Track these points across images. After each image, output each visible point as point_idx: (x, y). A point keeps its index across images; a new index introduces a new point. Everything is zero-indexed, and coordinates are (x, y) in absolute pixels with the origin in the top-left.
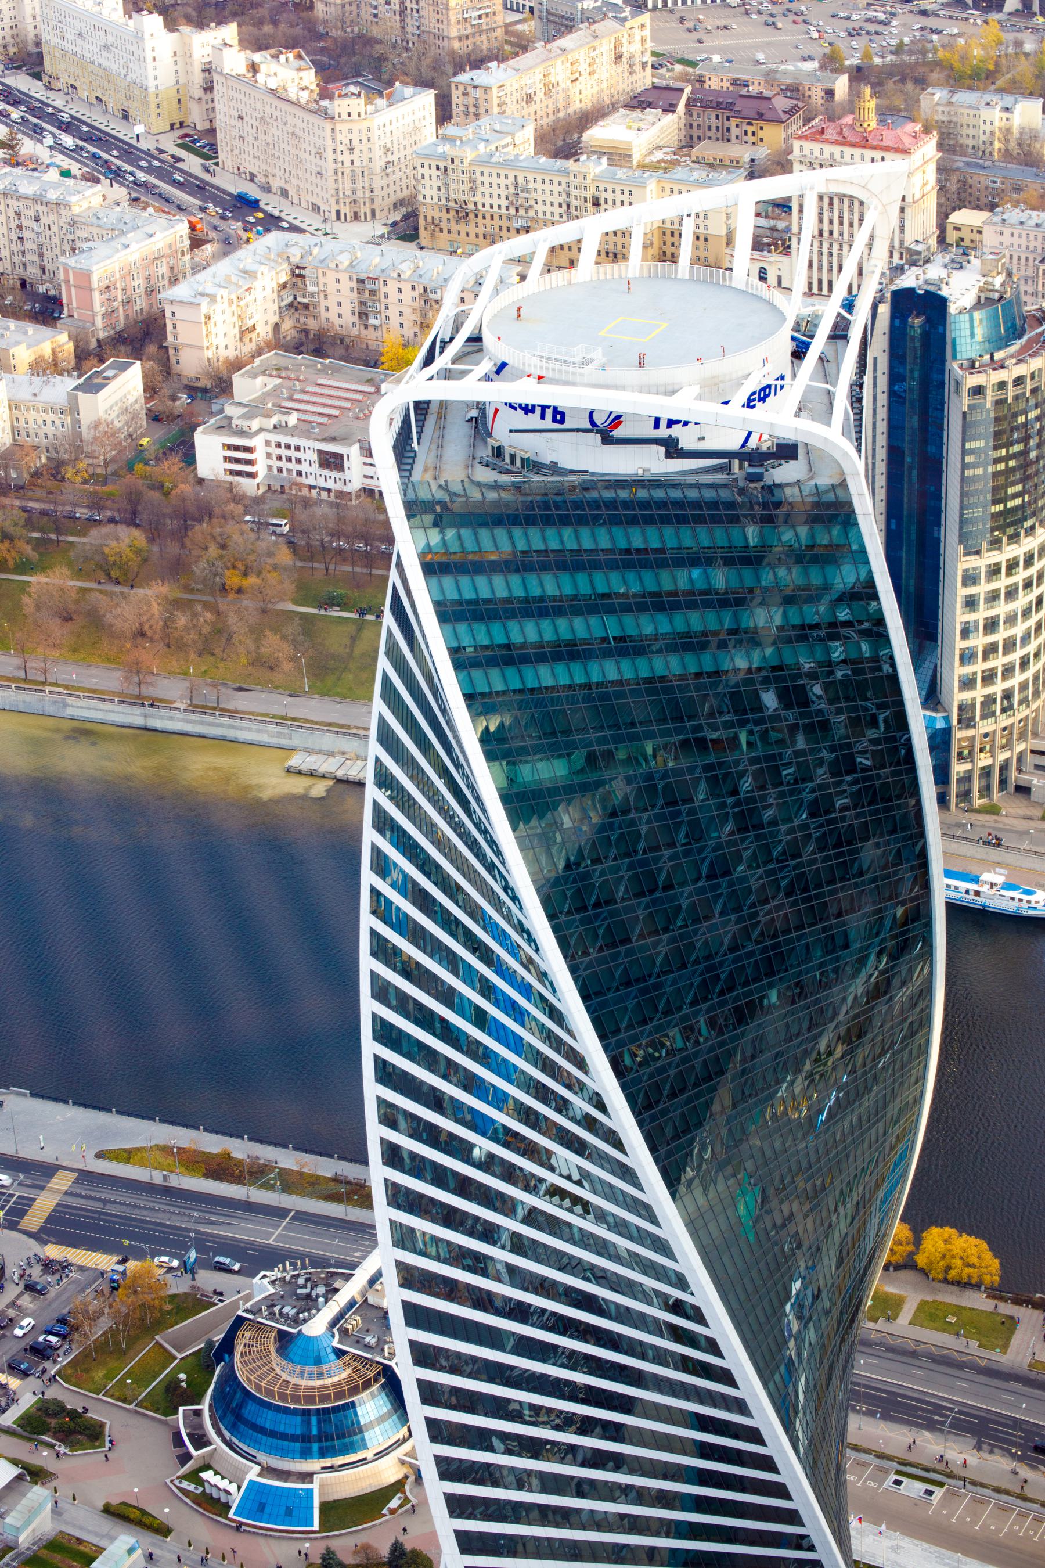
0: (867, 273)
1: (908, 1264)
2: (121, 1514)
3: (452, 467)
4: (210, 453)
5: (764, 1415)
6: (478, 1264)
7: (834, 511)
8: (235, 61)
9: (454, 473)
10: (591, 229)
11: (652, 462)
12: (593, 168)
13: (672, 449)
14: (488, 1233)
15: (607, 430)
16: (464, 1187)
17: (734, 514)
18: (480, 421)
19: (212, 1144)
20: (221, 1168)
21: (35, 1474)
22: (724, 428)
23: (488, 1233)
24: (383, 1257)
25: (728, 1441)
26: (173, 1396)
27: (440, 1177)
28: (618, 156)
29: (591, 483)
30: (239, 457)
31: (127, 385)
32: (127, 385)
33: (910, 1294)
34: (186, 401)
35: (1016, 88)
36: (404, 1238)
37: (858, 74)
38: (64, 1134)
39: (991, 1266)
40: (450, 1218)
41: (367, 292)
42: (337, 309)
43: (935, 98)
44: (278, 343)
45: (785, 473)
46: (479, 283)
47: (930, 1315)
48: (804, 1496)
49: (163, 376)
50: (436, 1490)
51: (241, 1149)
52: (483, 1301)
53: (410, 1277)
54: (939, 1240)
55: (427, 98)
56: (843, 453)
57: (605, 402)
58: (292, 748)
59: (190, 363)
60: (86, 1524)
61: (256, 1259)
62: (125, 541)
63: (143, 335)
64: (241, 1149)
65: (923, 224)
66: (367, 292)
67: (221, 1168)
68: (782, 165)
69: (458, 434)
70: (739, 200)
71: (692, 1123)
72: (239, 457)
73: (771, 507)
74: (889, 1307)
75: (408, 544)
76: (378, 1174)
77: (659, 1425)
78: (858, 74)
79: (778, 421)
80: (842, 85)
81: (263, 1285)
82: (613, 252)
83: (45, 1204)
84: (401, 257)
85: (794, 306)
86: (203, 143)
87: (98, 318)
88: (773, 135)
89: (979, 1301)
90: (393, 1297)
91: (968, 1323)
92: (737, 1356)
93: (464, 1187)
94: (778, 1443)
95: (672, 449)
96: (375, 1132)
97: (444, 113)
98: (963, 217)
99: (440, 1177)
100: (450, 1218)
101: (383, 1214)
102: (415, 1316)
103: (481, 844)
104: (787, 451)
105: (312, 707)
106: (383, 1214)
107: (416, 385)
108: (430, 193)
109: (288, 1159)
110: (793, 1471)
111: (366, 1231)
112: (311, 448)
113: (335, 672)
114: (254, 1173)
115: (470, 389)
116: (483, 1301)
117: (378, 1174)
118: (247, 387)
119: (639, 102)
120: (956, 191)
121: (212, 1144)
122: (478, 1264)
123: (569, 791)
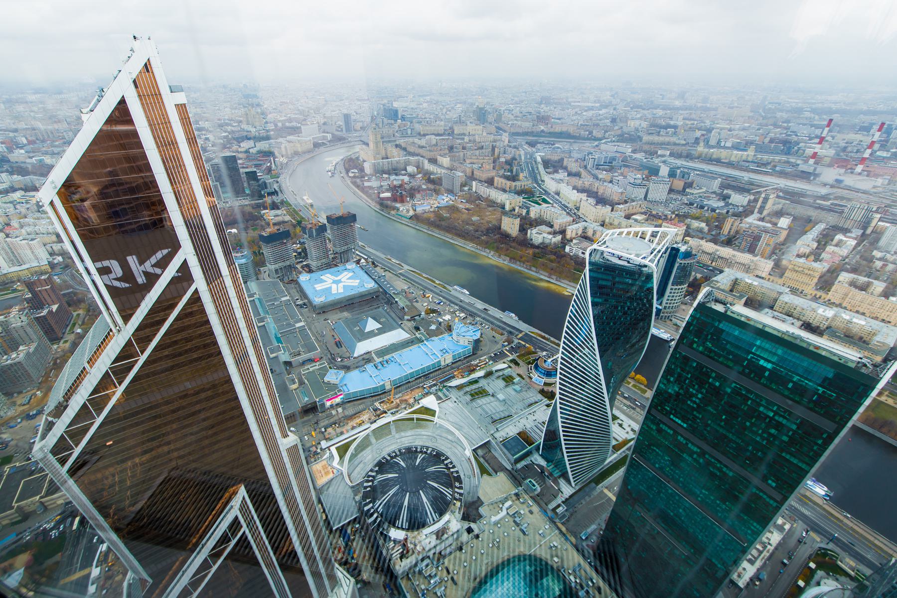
0: (666, 243)
1: (633, 378)
2: (519, 375)
3: (597, 258)
4: (567, 249)
5: (605, 391)
6: (572, 360)
7: (649, 277)
8: (585, 198)
9: (597, 259)
10: (626, 230)
11: (626, 264)
12: (631, 221)
13: (629, 262)
14: (574, 356)
15: (620, 258)
16: (572, 349)
17: (638, 274)
18: (602, 253)
19: (543, 334)
20: (544, 337)
21: (510, 367)
22: (639, 260)
23: (574, 356)
24: (560, 355)
25: (599, 393)
26: (529, 363)
27: (570, 347)
28: (636, 220)
29: (616, 264)
30: (571, 250)
31: (559, 238)
32: (559, 238)
33: (632, 383)
34: (565, 242)
35: (702, 221)
36: (563, 353)
37: (677, 215)
38: (154, 595)
39: (646, 382)
40: (570, 353)
41: (595, 232)
42: (590, 233)
43: (688, 221)
44: (581, 236)
45: (644, 269)
46: (608, 234)
47: (634, 386)
48: (608, 407)
49: (564, 238)
50: (558, 386)
51: (547, 336)
52: (571, 364)
53: (562, 358)
54: (638, 376)
55: (610, 208)
56: (655, 268)
57: (620, 254)
58: (568, 289)
59: (568, 237)
60: (514, 375)
61: (543, 350)
62: (553, 257)
63: (563, 232)
64: (547, 336)
65: (679, 238)
66: (595, 232)
67: (544, 337)
68: (660, 226)
69: (599, 254)
70: (650, 230)
71: (605, 351)
72: (571, 250)
73: (640, 273)
74: (629, 383)
75: (587, 268)
76: (562, 344)
77: (590, 388)
78: (677, 215)
79: (646, 262)
80: (673, 216)
81: (544, 353)
82: (629, 233)
83: (520, 335)
84: (601, 228)
85: (653, 246)
86: (578, 209)
87: (557, 227)
88: (660, 221)
89: (643, 387)
90: (560, 360)
91: (640, 389)
92: (603, 382)
93: (572, 349)
94: (606, 395)
95: (629, 262)
96: (563, 339)
97: (612, 210)
98: (687, 238)
99: (570, 347)
100: (570, 353)
101: (561, 349)
102: (561, 363)
103: (587, 307)
104: (645, 266)
105: (572, 284)
106: (561, 349)
107: (595, 246)
108: (607, 221)
109: (552, 339)
110: (607, 399)
111: (559, 345)
112: (581, 251)
113: (575, 280)
114: (547, 339)
115: (602, 248)
116: (571, 364)
117: (562, 344)
118: (575, 241)
119: (642, 213)
120: (687, 234)
121: (543, 334)
122: (572, 360)
123: (601, 304)
